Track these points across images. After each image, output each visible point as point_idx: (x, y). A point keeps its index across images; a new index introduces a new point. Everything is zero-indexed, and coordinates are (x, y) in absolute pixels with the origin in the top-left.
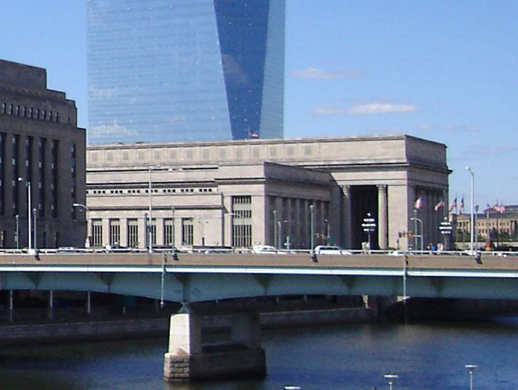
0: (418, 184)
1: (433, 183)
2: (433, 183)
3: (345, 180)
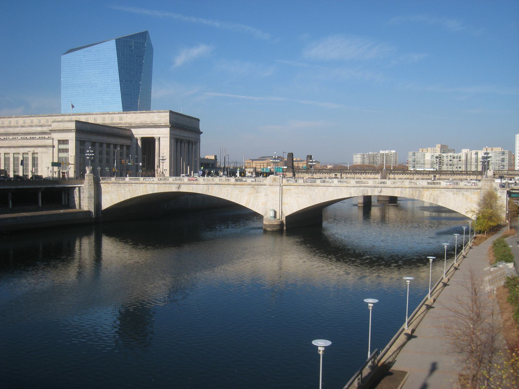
0: (178, 137)
1: (188, 138)
2: (188, 138)
3: (139, 134)
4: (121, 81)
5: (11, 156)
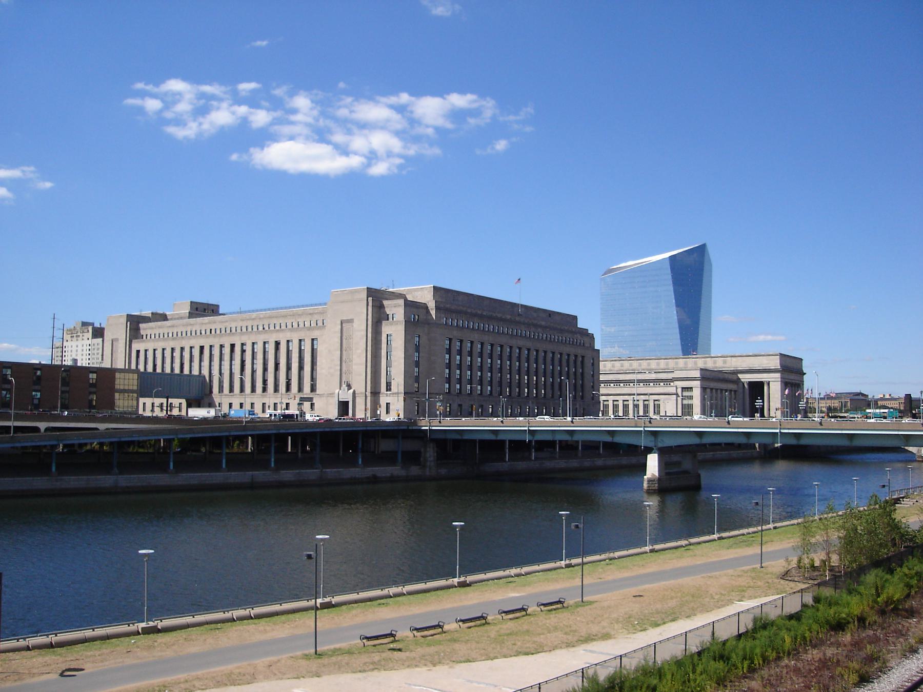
0: (787, 380)
3: (746, 378)
4: (682, 339)
5: (610, 404)
